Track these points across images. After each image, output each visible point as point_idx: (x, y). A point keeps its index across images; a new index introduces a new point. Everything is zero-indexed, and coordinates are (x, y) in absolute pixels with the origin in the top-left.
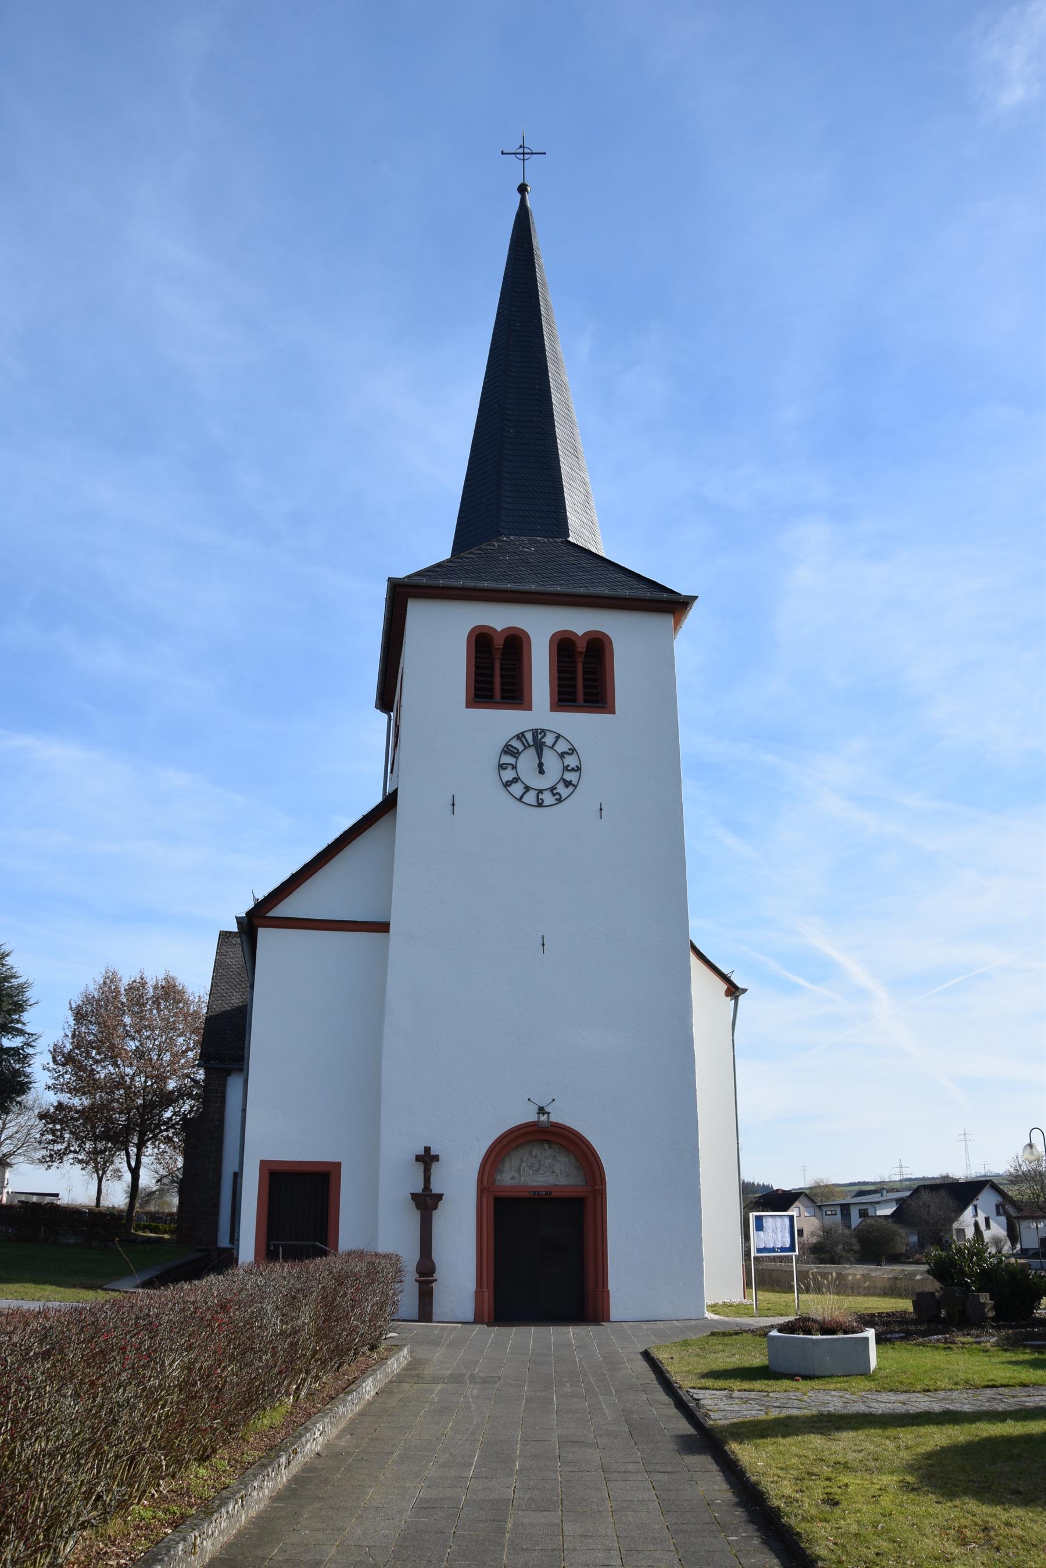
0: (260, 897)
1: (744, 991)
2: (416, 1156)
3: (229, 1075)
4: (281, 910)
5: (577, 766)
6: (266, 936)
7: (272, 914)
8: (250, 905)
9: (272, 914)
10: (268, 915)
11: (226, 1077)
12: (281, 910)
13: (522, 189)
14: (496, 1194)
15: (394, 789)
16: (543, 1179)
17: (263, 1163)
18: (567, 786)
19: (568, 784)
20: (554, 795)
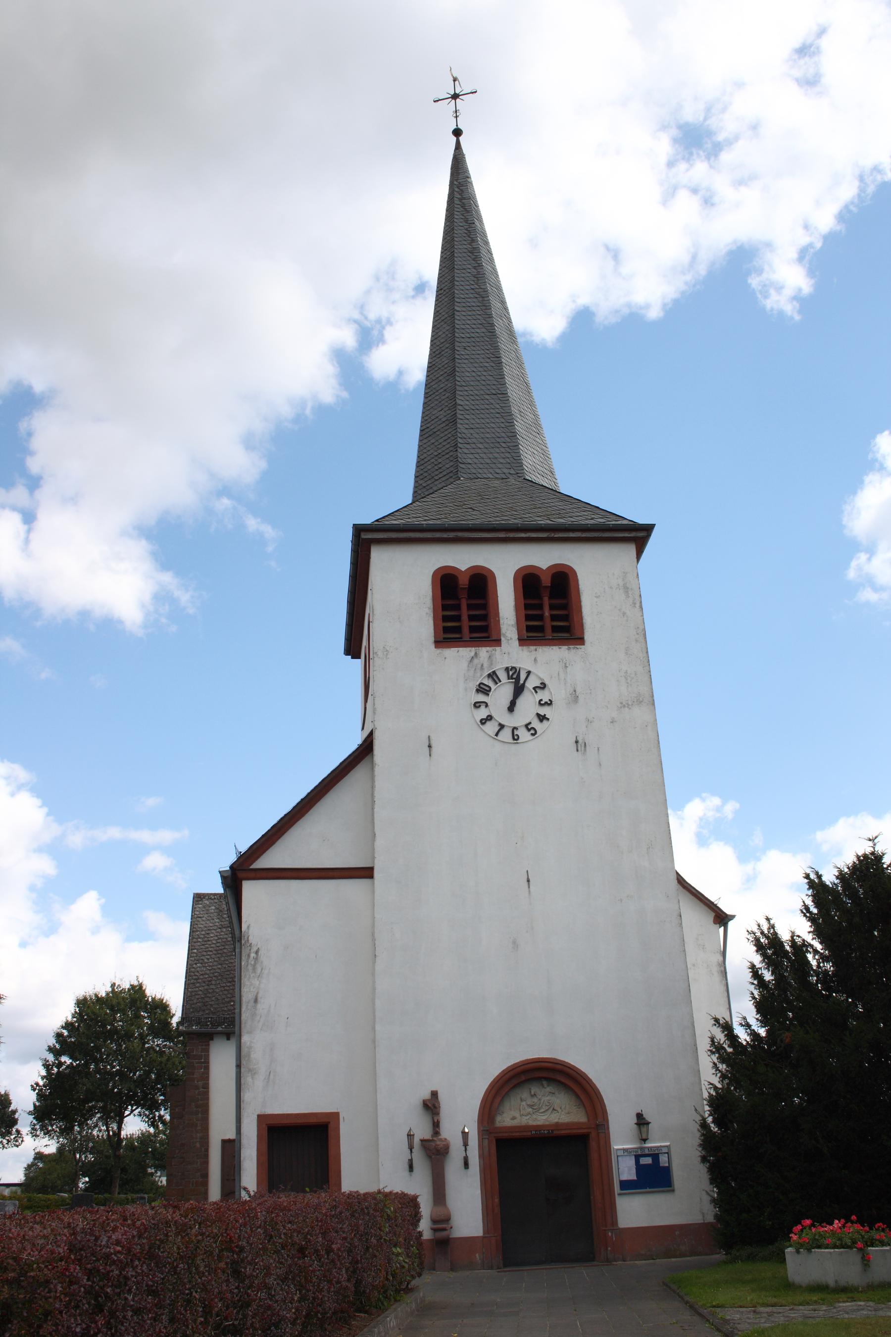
0: (243, 849)
1: (732, 917)
2: (432, 1091)
3: (212, 1039)
4: (267, 861)
5: (550, 700)
6: (251, 890)
7: (256, 865)
8: (233, 858)
9: (256, 865)
10: (252, 867)
11: (208, 1042)
12: (267, 861)
13: (457, 133)
14: (501, 1135)
15: (370, 730)
16: (544, 1118)
17: (260, 1117)
18: (541, 721)
19: (515, 738)
20: (529, 730)
